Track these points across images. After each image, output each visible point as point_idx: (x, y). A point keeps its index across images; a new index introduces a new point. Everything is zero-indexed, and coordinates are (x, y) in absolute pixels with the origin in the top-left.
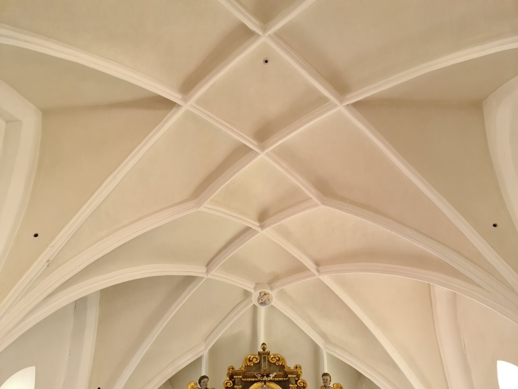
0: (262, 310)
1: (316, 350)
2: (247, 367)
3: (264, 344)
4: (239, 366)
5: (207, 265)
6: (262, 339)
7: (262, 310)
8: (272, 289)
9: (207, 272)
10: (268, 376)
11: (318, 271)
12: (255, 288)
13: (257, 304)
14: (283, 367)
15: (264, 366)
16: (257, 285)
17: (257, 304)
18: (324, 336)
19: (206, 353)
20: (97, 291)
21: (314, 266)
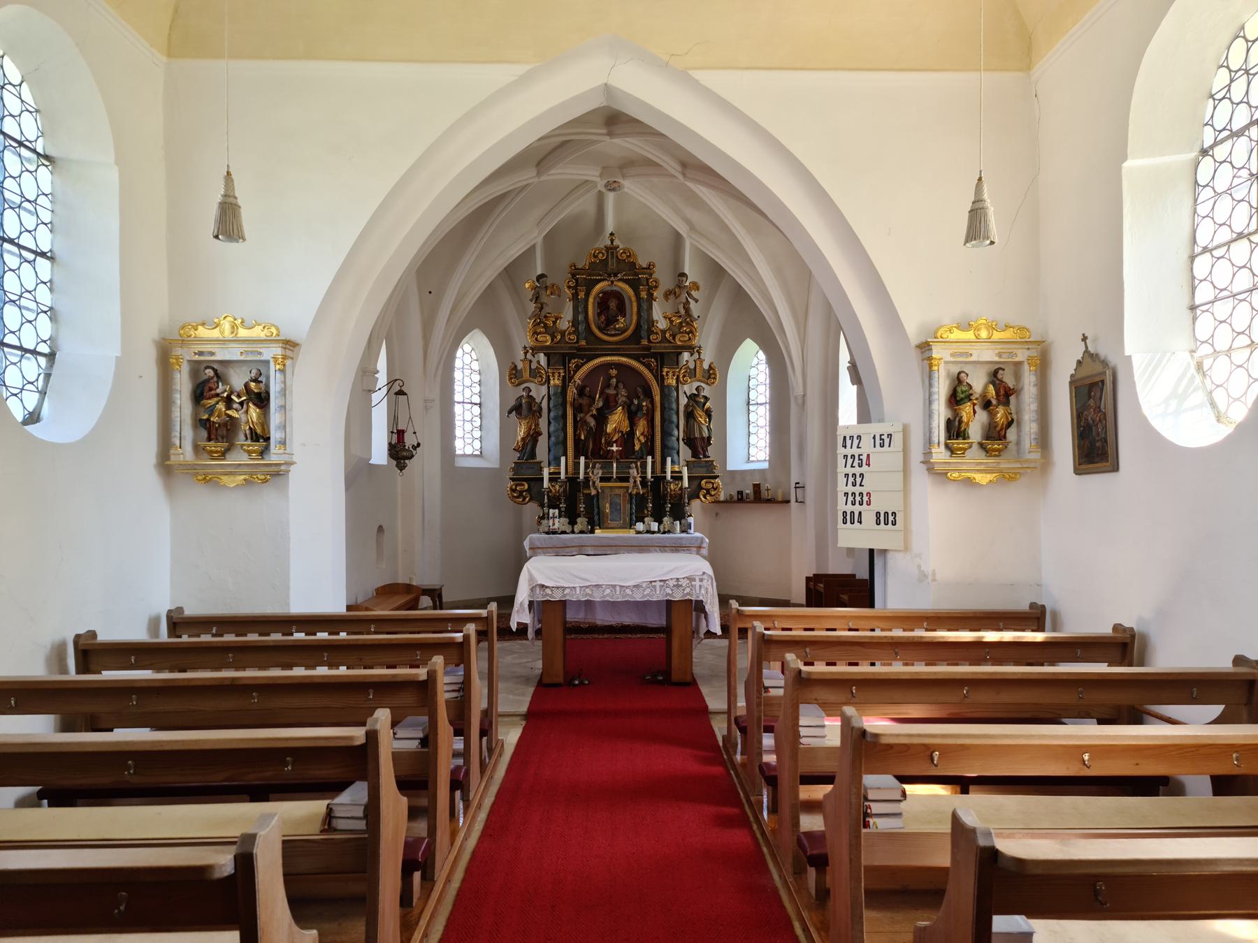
0: (610, 198)
1: (678, 238)
2: (591, 264)
3: (612, 234)
4: (583, 263)
5: (538, 165)
6: (610, 226)
7: (610, 198)
8: (624, 177)
9: (539, 174)
10: (616, 275)
11: (684, 175)
12: (601, 176)
13: (603, 190)
14: (634, 264)
15: (612, 265)
16: (605, 170)
17: (603, 190)
18: (692, 227)
19: (539, 240)
20: (946, 883)
21: (679, 168)
